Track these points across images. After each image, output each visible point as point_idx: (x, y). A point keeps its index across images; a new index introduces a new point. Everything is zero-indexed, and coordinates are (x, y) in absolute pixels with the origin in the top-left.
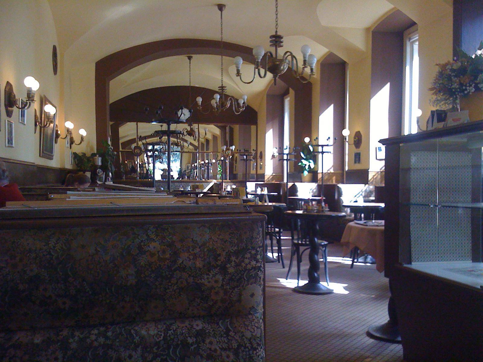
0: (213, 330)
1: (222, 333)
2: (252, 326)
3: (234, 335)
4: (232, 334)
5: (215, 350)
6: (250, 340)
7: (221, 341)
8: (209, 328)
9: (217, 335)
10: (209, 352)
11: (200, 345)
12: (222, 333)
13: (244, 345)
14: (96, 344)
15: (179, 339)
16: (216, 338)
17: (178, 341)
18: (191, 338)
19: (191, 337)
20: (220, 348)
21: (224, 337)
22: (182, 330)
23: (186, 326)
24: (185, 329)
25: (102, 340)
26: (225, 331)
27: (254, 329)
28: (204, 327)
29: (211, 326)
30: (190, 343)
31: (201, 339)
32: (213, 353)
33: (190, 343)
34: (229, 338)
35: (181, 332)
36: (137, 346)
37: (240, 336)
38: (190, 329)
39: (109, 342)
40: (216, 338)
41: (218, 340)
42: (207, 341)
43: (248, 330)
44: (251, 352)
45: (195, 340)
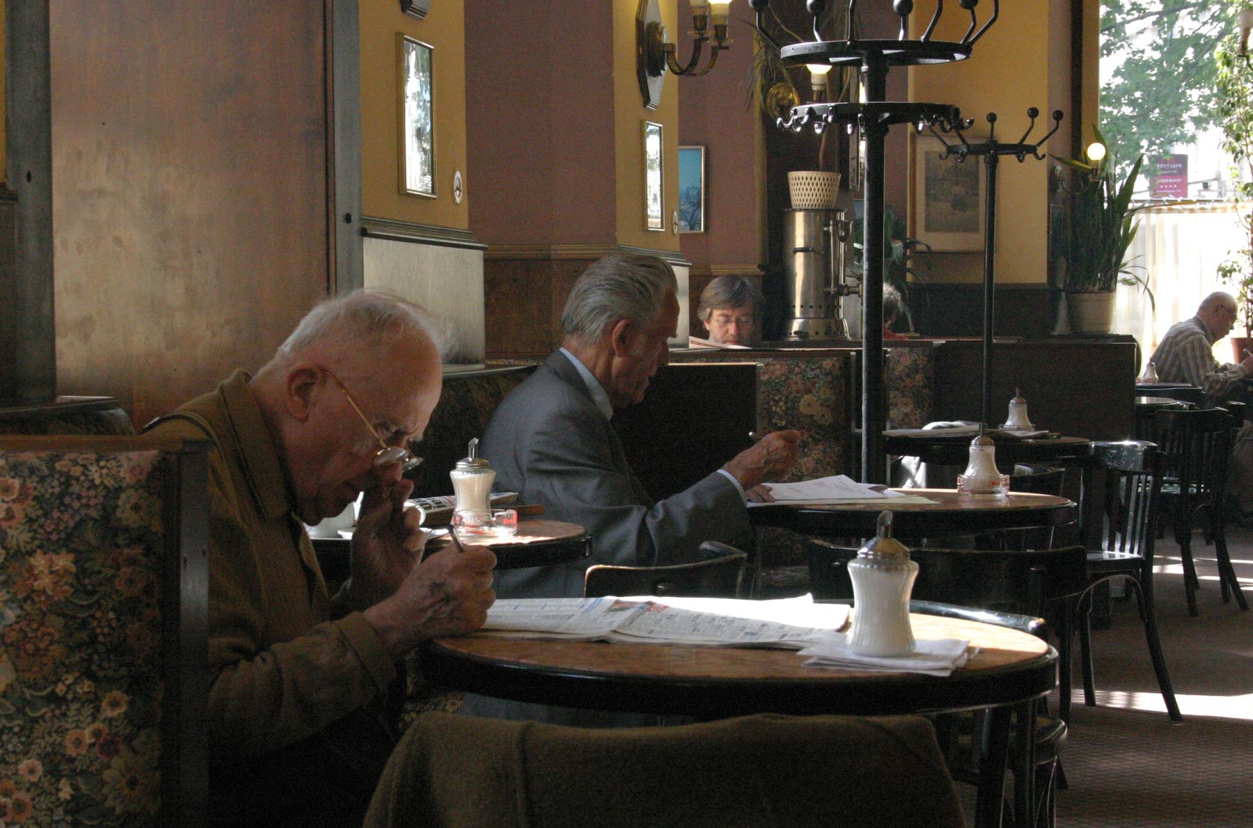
0: (49, 733)
1: (57, 712)
2: (36, 637)
3: (63, 683)
4: (60, 689)
5: (97, 734)
6: (72, 649)
7: (76, 718)
8: (43, 745)
9: (60, 727)
10: (96, 749)
11: (78, 770)
12: (57, 712)
13: (85, 664)
14: (784, 408)
15: (63, 820)
16: (68, 730)
17: (66, 822)
18: (61, 790)
19: (58, 790)
20: (93, 722)
21: (68, 709)
22: (41, 811)
23: (33, 799)
24: (38, 802)
25: (781, 404)
26: (52, 706)
27: (44, 634)
28: (39, 755)
29: (38, 737)
30: (72, 792)
31: (67, 767)
32: (102, 740)
33: (72, 792)
34: (70, 696)
35: (45, 812)
36: (788, 378)
37: (64, 670)
38: (39, 791)
39: (783, 398)
40: (68, 730)
41: (74, 725)
42: (71, 752)
43: (46, 649)
44: (101, 648)
45: (64, 781)
